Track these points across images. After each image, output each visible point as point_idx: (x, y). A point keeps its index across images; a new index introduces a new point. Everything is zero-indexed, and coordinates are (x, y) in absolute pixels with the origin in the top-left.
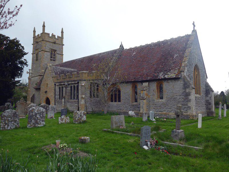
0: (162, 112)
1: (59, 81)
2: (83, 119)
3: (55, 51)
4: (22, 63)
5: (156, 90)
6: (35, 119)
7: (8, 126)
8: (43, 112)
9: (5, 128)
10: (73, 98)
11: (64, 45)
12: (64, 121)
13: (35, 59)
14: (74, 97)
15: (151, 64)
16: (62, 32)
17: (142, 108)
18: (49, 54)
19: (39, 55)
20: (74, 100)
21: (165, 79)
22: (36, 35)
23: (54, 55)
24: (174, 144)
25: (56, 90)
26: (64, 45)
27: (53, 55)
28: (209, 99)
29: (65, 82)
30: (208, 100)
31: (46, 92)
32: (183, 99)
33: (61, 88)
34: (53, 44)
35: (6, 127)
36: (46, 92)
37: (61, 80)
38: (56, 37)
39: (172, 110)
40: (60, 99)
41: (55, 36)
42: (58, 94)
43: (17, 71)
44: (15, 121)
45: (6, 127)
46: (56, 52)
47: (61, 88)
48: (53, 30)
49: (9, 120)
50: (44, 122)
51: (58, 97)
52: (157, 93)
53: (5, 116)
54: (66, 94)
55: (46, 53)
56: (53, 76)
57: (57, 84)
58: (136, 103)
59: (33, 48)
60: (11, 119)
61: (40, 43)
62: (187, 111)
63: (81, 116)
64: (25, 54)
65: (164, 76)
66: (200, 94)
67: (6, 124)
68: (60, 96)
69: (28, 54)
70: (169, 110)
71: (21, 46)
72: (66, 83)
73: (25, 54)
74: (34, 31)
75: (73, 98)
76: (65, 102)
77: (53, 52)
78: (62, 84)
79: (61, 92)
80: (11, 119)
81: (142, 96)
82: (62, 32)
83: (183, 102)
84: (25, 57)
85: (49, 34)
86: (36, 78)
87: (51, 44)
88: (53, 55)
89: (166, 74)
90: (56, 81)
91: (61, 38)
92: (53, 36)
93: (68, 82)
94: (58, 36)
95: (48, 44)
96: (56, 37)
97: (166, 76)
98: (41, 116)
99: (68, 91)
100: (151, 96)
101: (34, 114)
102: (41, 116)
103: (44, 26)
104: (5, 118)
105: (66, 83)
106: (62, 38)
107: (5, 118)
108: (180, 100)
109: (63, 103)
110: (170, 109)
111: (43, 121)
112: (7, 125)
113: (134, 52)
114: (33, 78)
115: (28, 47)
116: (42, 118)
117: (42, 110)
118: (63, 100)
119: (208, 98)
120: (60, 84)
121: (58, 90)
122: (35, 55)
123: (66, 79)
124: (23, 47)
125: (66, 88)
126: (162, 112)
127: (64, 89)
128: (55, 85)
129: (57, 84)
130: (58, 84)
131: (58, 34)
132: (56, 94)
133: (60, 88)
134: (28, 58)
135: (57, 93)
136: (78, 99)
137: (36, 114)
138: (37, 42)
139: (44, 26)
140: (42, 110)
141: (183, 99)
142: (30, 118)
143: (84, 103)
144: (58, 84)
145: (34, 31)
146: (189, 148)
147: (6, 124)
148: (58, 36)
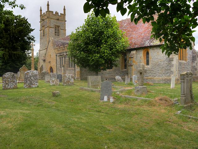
0: (148, 76)
1: (59, 52)
2: (71, 81)
3: (59, 27)
4: (29, 38)
5: (143, 57)
6: (29, 80)
7: (8, 85)
8: (36, 75)
9: (6, 87)
10: (70, 66)
11: (66, 21)
12: (55, 83)
13: (42, 34)
14: (72, 66)
15: (139, 33)
16: (64, 10)
17: (130, 74)
18: (53, 29)
19: (45, 31)
20: (72, 68)
21: (151, 47)
22: (42, 13)
23: (58, 30)
24: (148, 99)
25: (57, 60)
26: (66, 21)
27: (57, 31)
28: (195, 65)
29: (64, 53)
30: (194, 66)
31: (50, 62)
32: (166, 65)
33: (61, 58)
34: (57, 20)
35: (7, 86)
36: (50, 62)
37: (61, 51)
38: (59, 14)
39: (157, 75)
40: (60, 68)
41: (58, 13)
42: (59, 63)
43: (26, 46)
44: (14, 82)
45: (7, 86)
46: (59, 28)
47: (61, 58)
48: (56, 8)
49: (9, 81)
50: (37, 83)
51: (59, 66)
52: (143, 60)
53: (6, 78)
54: (65, 63)
55: (51, 29)
56: (55, 48)
57: (58, 55)
58: (125, 69)
59: (41, 26)
60: (11, 79)
61: (45, 20)
62: (170, 75)
63: (69, 78)
64: (32, 30)
65: (150, 44)
66: (186, 60)
67: (7, 84)
68: (60, 65)
69: (34, 30)
70: (154, 75)
71: (28, 23)
72: (65, 54)
73: (32, 30)
74: (41, 10)
75: (70, 66)
76: (64, 70)
77: (57, 28)
78: (62, 54)
79: (61, 62)
80: (11, 79)
81: (130, 62)
82: (64, 10)
83: (167, 67)
84: (31, 34)
85: (53, 12)
86: (44, 51)
87: (55, 20)
88: (57, 31)
89: (152, 42)
90: (57, 52)
91: (64, 15)
92: (57, 13)
93: (66, 52)
94: (60, 13)
95: (52, 20)
96: (59, 14)
97: (152, 44)
98: (35, 78)
99: (66, 60)
100: (138, 62)
101: (29, 76)
102: (35, 78)
103: (48, 5)
104: (6, 79)
105: (64, 53)
106: (64, 15)
107: (6, 79)
108: (164, 65)
109: (63, 71)
110: (155, 74)
111: (36, 82)
112: (7, 85)
113: (125, 23)
114: (41, 52)
115: (35, 23)
116: (35, 80)
117: (35, 74)
118: (63, 69)
119: (194, 64)
120: (60, 54)
121: (59, 60)
122: (42, 31)
123: (64, 50)
124: (30, 24)
125: (65, 57)
126: (148, 76)
127: (63, 58)
128: (56, 55)
129: (58, 55)
130: (59, 55)
131: (61, 11)
132: (57, 63)
133: (60, 58)
134: (36, 33)
135: (59, 63)
136: (75, 67)
137: (31, 77)
138: (43, 20)
139: (48, 5)
140: (35, 74)
141: (166, 65)
142: (26, 79)
143: (79, 70)
144: (59, 55)
145: (41, 10)
146: (147, 97)
147: (7, 84)
148: (60, 13)
